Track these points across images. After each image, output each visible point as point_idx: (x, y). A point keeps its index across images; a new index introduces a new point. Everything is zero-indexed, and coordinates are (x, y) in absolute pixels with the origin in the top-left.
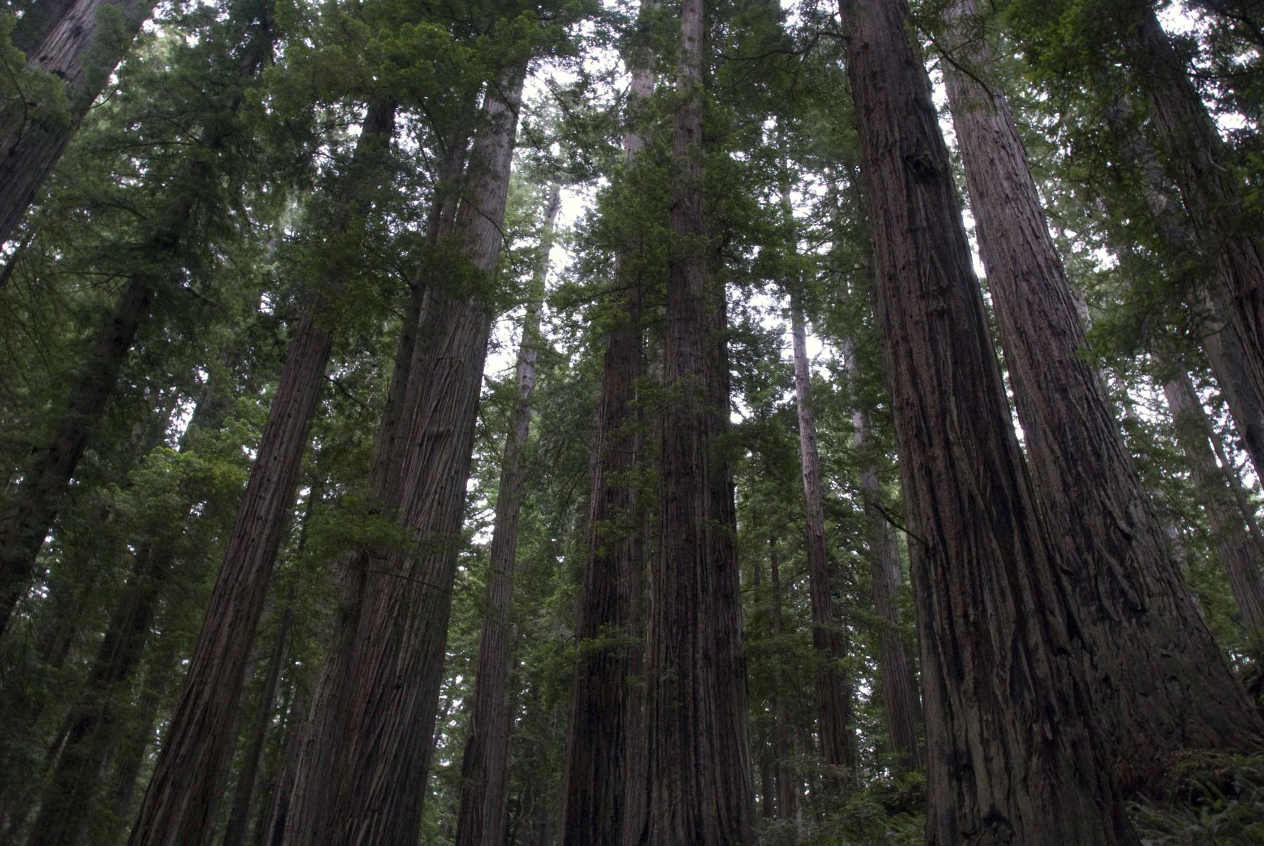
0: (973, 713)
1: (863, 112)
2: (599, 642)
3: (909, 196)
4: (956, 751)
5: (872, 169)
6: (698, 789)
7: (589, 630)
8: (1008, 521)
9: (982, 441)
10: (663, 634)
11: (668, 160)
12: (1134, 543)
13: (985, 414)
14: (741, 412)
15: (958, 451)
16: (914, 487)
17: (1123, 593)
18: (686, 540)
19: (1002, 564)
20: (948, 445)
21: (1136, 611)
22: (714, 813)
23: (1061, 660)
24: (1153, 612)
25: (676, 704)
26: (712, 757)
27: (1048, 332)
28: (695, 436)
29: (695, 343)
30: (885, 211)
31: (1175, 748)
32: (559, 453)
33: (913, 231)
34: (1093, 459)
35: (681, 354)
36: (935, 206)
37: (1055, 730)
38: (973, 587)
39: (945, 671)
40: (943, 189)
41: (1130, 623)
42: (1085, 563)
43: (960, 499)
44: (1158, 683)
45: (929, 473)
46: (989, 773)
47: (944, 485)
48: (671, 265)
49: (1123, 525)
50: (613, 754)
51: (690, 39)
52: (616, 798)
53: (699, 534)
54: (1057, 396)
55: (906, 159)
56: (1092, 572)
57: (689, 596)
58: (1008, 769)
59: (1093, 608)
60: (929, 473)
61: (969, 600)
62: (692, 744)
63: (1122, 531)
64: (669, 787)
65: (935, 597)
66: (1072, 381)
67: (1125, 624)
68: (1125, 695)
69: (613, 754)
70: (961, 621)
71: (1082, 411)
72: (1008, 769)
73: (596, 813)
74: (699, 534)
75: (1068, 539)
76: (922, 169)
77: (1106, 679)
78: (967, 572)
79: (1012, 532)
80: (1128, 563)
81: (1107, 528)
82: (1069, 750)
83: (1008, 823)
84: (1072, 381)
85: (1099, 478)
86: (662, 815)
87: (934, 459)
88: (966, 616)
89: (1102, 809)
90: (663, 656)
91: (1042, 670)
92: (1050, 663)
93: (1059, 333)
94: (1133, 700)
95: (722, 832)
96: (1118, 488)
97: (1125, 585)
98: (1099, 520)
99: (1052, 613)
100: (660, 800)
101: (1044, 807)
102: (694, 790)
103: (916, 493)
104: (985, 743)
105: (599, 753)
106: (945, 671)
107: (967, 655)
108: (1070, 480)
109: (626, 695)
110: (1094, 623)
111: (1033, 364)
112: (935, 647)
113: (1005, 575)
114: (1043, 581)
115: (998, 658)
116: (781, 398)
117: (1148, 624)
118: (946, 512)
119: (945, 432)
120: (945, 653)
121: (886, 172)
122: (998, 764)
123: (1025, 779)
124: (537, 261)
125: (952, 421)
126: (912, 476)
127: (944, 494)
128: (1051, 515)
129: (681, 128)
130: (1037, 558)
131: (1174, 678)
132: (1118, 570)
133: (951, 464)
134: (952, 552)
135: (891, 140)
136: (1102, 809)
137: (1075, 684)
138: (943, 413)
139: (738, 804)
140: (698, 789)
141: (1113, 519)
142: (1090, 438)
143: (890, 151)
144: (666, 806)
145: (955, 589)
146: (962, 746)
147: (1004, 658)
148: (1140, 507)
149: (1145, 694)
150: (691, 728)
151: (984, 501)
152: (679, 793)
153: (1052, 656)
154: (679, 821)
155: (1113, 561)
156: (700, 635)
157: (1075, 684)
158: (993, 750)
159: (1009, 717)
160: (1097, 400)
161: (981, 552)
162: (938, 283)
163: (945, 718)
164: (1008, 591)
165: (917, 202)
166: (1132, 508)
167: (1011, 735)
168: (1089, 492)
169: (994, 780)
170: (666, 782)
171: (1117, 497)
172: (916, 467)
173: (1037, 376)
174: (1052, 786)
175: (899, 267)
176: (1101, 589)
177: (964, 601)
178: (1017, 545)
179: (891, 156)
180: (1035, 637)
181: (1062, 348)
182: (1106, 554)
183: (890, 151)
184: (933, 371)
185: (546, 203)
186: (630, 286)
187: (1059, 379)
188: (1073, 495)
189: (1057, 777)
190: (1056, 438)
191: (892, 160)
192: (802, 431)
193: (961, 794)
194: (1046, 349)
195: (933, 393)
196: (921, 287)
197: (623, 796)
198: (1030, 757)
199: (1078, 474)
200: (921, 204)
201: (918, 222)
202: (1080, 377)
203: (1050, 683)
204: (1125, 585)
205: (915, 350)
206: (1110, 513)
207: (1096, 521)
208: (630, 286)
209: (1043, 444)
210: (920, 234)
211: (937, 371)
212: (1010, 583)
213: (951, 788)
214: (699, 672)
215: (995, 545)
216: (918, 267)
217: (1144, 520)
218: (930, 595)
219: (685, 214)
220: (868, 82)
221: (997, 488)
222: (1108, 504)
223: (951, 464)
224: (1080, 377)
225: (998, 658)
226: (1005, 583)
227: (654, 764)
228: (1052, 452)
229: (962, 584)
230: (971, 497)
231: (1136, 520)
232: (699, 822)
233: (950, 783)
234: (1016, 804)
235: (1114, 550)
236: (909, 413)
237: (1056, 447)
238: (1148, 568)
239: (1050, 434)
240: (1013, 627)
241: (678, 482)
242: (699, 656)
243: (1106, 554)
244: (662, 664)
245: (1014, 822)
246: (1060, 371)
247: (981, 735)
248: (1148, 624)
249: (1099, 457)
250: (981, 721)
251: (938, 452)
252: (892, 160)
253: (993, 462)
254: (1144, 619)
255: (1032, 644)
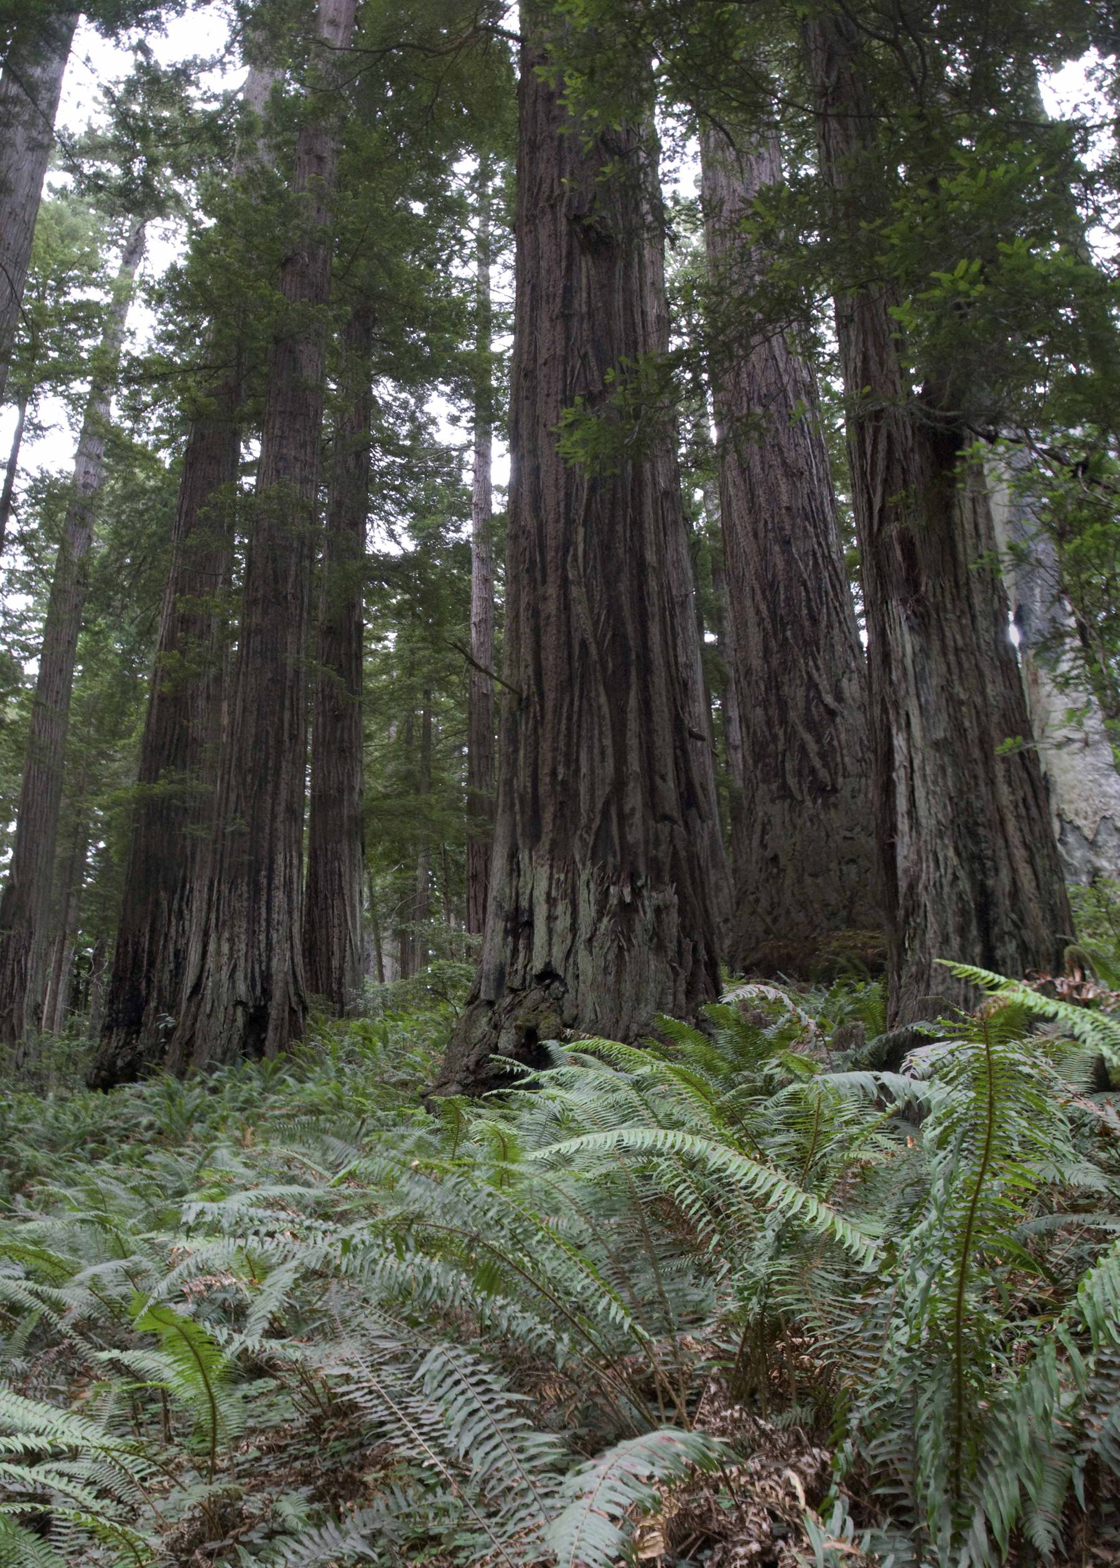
0: (543, 873)
1: (526, 149)
2: (160, 788)
3: (569, 269)
4: (517, 908)
5: (526, 229)
6: (269, 944)
7: (148, 774)
8: (627, 673)
9: (610, 583)
10: (233, 782)
11: (281, 196)
12: (838, 720)
13: (621, 551)
14: (388, 538)
15: (575, 592)
16: (517, 630)
17: (813, 771)
18: (271, 680)
19: (608, 721)
20: (565, 584)
21: (824, 791)
22: (287, 966)
23: (664, 828)
24: (846, 793)
25: (246, 857)
26: (290, 913)
27: (779, 472)
28: (294, 560)
29: (303, 446)
30: (533, 288)
31: (837, 928)
32: (138, 573)
33: (566, 317)
34: (807, 624)
35: (282, 458)
36: (603, 287)
37: (636, 893)
38: (568, 745)
39: (519, 830)
40: (620, 264)
41: (814, 801)
42: (775, 738)
43: (570, 646)
44: (833, 866)
45: (536, 613)
46: (550, 932)
47: (552, 630)
48: (277, 340)
49: (829, 699)
50: (175, 906)
51: (333, 23)
52: (177, 953)
53: (290, 674)
54: (777, 548)
55: (575, 219)
56: (780, 748)
57: (271, 742)
58: (574, 928)
59: (774, 787)
60: (536, 613)
61: (561, 758)
62: (264, 898)
63: (826, 706)
64: (231, 940)
65: (522, 753)
66: (799, 533)
67: (809, 803)
68: (791, 875)
69: (175, 906)
70: (547, 779)
71: (804, 569)
72: (574, 928)
73: (152, 964)
74: (290, 674)
75: (759, 711)
76: (593, 235)
77: (775, 859)
78: (563, 727)
79: (629, 687)
80: (825, 741)
81: (808, 702)
82: (650, 915)
83: (563, 982)
84: (799, 533)
85: (810, 646)
86: (219, 969)
87: (545, 599)
88: (554, 773)
89: (676, 974)
90: (232, 806)
91: (635, 834)
92: (647, 830)
93: (793, 474)
94: (800, 880)
95: (297, 989)
96: (833, 658)
97: (817, 763)
98: (801, 693)
99: (663, 778)
100: (219, 953)
101: (606, 968)
102: (263, 946)
103: (518, 638)
104: (551, 901)
105: (157, 903)
106: (519, 830)
107: (548, 816)
108: (773, 644)
109: (194, 846)
110: (773, 801)
111: (753, 508)
112: (513, 805)
113: (609, 734)
114: (659, 742)
115: (584, 821)
116: (458, 530)
117: (835, 806)
118: (550, 659)
119: (564, 569)
120: (523, 812)
121: (543, 234)
122: (563, 923)
123: (590, 940)
124: (107, 320)
125: (575, 556)
126: (517, 616)
127: (550, 639)
128: (744, 684)
129: (308, 152)
130: (656, 718)
131: (853, 861)
132: (812, 747)
133: (566, 605)
134: (549, 704)
135: (557, 192)
136: (676, 974)
137: (675, 854)
138: (567, 545)
139: (341, 969)
140: (269, 944)
141: (818, 691)
142: (809, 600)
143: (552, 206)
144: (225, 959)
145: (545, 746)
146: (524, 904)
147: (591, 820)
148: (855, 682)
149: (814, 875)
150: (264, 881)
151: (599, 653)
152: (243, 946)
153: (651, 823)
154: (240, 975)
155: (808, 738)
156: (283, 786)
157: (675, 854)
158: (560, 908)
159: (584, 877)
160: (828, 558)
161: (585, 707)
162: (587, 386)
163: (510, 874)
164: (610, 751)
165: (579, 280)
166: (845, 681)
167: (583, 894)
168: (794, 661)
169: (555, 939)
170: (226, 935)
171: (829, 669)
172: (523, 606)
173: (756, 522)
174: (620, 948)
175: (541, 361)
176: (788, 766)
177: (554, 758)
178: (633, 702)
179: (554, 213)
180: (635, 799)
181: (794, 492)
182: (800, 728)
183: (552, 206)
184: (562, 494)
185: (122, 242)
186: (225, 365)
187: (782, 529)
188: (775, 662)
189: (629, 940)
190: (765, 598)
191: (555, 219)
192: (475, 570)
193: (515, 952)
194: (773, 494)
195: (557, 521)
196: (564, 391)
197: (186, 951)
198: (600, 920)
199: (785, 639)
200: (584, 281)
201: (576, 306)
202: (811, 529)
203: (641, 849)
204: (817, 763)
205: (543, 468)
206: (816, 686)
207: (796, 694)
208: (225, 365)
209: (748, 603)
210: (575, 321)
211: (568, 495)
212: (614, 742)
213: (505, 944)
214: (279, 825)
215: (603, 699)
216: (565, 363)
217: (857, 695)
218: (516, 751)
219: (303, 275)
220: (540, 106)
221: (619, 637)
222: (815, 675)
223: (566, 605)
224: (811, 529)
225: (584, 821)
226: (608, 742)
227: (213, 916)
228: (758, 612)
229: (555, 739)
230: (583, 644)
231: (847, 694)
232: (267, 977)
233: (505, 939)
234: (575, 964)
235: (812, 726)
236: (523, 543)
237: (763, 607)
238: (849, 747)
239: (758, 592)
240: (608, 789)
241: (265, 613)
242: (281, 809)
243: (800, 728)
244: (231, 815)
245: (569, 979)
246: (786, 519)
247: (549, 894)
248: (835, 806)
249: (814, 621)
250: (551, 878)
251: (552, 590)
252: (555, 219)
253: (621, 608)
254: (832, 799)
255: (627, 809)
